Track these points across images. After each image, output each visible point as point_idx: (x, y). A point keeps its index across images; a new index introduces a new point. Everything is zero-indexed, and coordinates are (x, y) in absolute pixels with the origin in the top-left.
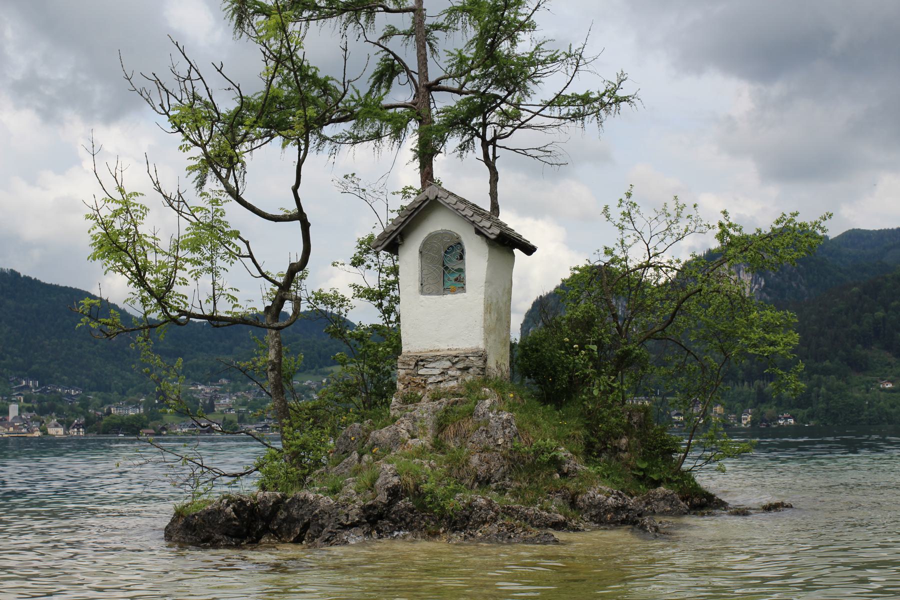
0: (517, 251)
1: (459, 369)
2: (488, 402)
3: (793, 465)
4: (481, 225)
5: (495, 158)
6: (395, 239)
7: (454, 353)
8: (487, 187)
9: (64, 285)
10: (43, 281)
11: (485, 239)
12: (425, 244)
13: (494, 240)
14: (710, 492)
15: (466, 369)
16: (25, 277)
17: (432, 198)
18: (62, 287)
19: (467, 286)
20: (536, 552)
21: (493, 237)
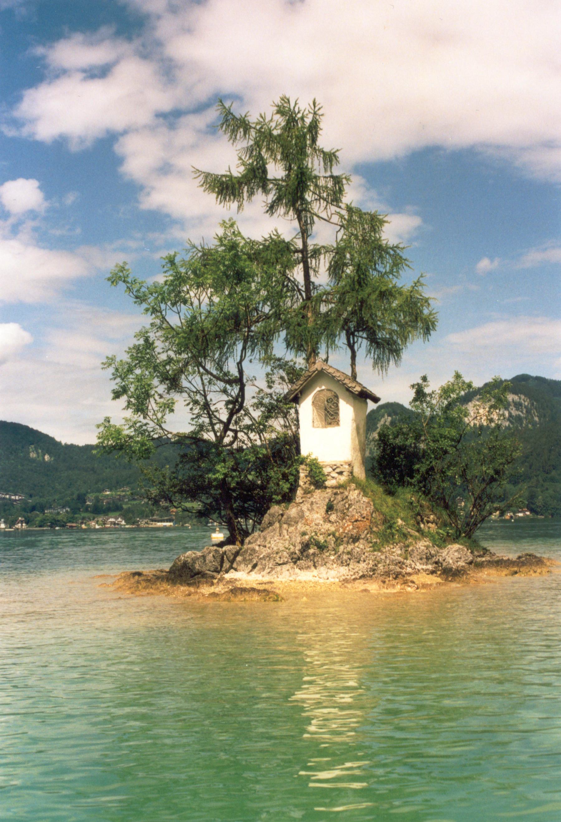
0: (369, 401)
1: (337, 473)
2: (354, 494)
3: (502, 545)
4: (350, 385)
5: (354, 343)
6: (297, 394)
7: (334, 463)
8: (350, 361)
9: (84, 445)
10: (58, 439)
11: (425, 755)
12: (315, 398)
13: (357, 395)
14: (512, 542)
15: (341, 473)
16: (66, 444)
17: (319, 369)
18: (83, 447)
19: (341, 423)
20: (406, 772)
21: (357, 393)
